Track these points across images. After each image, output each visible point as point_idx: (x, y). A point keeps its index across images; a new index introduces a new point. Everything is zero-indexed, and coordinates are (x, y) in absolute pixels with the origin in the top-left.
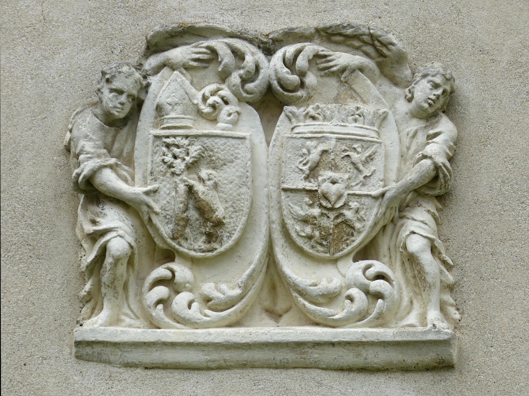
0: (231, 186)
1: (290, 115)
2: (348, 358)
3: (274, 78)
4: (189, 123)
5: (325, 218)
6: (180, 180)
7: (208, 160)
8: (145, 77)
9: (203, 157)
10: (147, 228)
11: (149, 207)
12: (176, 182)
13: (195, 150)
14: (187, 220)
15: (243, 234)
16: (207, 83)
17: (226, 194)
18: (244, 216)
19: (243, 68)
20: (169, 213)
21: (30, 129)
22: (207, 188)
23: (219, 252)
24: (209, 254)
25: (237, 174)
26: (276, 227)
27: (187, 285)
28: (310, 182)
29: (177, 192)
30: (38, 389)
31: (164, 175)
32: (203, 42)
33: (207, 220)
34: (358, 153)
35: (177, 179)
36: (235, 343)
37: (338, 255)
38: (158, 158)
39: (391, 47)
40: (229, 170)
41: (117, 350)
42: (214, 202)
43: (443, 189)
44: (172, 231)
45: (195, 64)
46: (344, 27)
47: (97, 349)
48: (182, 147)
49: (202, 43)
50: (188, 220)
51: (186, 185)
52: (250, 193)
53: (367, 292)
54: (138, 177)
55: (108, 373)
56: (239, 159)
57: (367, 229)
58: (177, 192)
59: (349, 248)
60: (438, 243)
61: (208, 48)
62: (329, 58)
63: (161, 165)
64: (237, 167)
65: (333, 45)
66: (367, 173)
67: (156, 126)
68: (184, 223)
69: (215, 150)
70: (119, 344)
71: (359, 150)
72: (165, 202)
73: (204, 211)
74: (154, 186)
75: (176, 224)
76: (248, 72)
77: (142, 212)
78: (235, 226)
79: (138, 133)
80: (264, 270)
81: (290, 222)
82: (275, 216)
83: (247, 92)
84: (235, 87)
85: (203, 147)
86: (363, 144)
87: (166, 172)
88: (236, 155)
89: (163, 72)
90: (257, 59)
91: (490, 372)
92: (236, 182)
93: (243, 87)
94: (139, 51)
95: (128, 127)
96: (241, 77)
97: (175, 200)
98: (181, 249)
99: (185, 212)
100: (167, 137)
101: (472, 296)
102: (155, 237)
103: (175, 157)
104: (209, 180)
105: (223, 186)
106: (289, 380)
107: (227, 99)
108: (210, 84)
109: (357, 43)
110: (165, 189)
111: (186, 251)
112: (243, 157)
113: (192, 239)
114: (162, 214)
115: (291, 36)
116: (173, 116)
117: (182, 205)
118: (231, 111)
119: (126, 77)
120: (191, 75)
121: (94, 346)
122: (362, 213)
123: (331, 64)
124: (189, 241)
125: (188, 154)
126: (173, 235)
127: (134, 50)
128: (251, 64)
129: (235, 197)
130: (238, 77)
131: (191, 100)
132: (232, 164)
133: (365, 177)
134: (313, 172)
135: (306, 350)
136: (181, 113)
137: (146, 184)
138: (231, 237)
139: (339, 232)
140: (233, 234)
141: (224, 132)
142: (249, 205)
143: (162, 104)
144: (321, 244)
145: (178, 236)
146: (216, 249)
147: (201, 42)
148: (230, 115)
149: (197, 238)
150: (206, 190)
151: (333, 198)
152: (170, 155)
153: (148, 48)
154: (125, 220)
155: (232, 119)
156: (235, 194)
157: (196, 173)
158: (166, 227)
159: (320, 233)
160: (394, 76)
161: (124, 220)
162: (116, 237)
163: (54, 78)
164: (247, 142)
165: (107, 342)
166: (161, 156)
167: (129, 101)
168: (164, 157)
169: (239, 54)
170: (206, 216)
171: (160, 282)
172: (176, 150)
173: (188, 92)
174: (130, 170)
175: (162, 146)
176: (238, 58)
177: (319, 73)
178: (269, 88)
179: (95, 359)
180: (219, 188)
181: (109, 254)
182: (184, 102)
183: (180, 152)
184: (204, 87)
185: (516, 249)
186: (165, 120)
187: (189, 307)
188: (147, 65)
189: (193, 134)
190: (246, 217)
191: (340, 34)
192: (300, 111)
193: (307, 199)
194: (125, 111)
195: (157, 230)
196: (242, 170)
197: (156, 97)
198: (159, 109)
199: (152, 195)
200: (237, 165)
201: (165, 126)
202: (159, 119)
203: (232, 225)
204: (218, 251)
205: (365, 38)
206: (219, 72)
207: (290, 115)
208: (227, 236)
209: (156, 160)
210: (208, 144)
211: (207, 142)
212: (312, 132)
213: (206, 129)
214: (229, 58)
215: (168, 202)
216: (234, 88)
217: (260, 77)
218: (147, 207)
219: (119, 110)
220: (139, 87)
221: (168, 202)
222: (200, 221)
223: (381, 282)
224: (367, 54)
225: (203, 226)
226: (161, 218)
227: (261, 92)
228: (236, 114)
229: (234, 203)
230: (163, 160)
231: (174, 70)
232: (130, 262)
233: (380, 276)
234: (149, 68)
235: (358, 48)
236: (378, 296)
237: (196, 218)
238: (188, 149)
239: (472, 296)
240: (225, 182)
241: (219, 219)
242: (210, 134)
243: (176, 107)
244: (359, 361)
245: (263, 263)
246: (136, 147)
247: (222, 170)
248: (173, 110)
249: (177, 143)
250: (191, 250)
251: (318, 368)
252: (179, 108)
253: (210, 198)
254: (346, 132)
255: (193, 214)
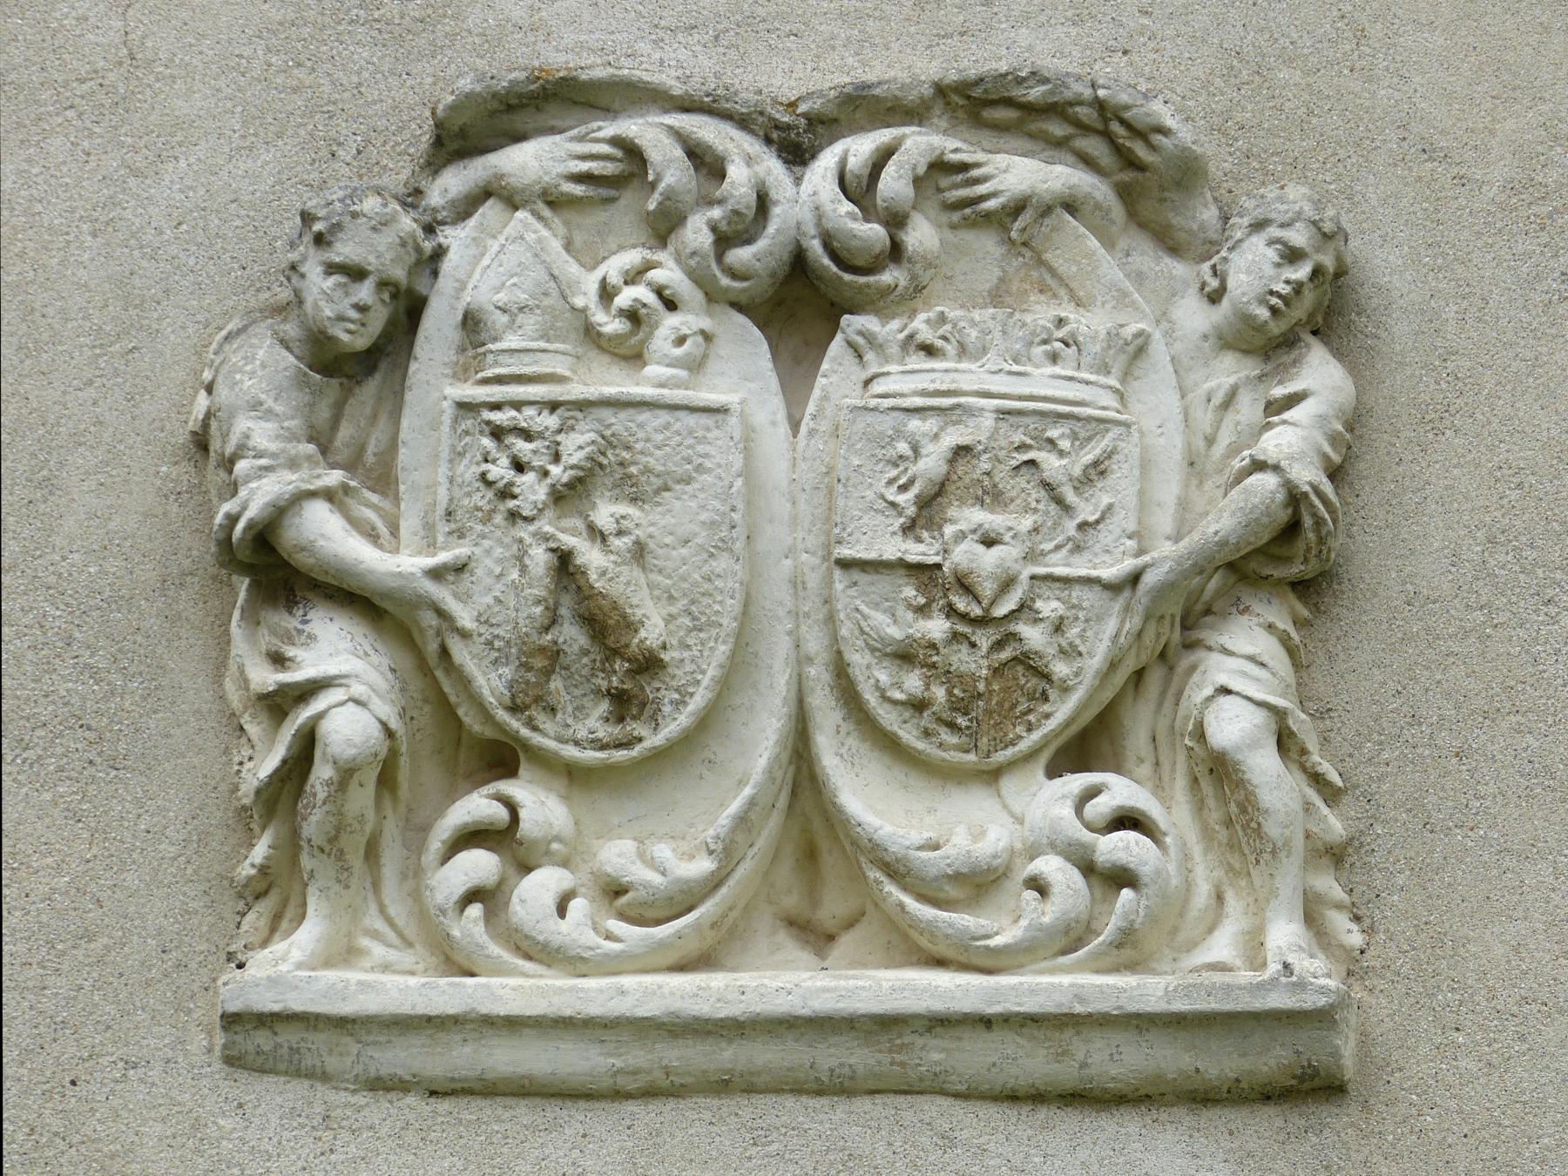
0: (684, 551)
1: (860, 340)
2: (1032, 1062)
3: (813, 232)
4: (560, 367)
5: (964, 648)
6: (534, 535)
7: (618, 476)
8: (429, 229)
9: (601, 466)
10: (435, 679)
11: (441, 613)
12: (521, 541)
13: (577, 445)
14: (554, 655)
15: (719, 695)
16: (614, 247)
17: (669, 577)
18: (724, 642)
19: (720, 202)
20: (502, 633)
21: (90, 383)
22: (612, 558)
23: (650, 750)
24: (621, 755)
25: (704, 517)
26: (819, 674)
27: (555, 846)
28: (919, 540)
29: (524, 570)
30: (113, 1156)
31: (487, 519)
32: (601, 123)
33: (614, 653)
34: (1062, 454)
35: (524, 532)
36: (696, 1019)
37: (1001, 756)
38: (468, 471)
39: (1158, 139)
40: (678, 504)
41: (348, 1039)
42: (635, 601)
43: (1313, 561)
44: (511, 685)
45: (578, 190)
46: (1020, 81)
47: (289, 1036)
48: (541, 435)
49: (600, 129)
50: (558, 652)
51: (553, 550)
52: (740, 574)
53: (1088, 868)
54: (409, 525)
55: (319, 1109)
56: (709, 471)
57: (1088, 679)
58: (524, 570)
59: (1036, 736)
60: (1300, 722)
61: (616, 141)
62: (975, 173)
63: (478, 490)
64: (702, 496)
65: (987, 133)
66: (1087, 513)
67: (462, 373)
68: (546, 663)
69: (639, 446)
70: (354, 1021)
71: (1065, 444)
72: (489, 600)
73: (604, 625)
74: (457, 551)
75: (522, 665)
76: (736, 212)
77: (421, 631)
78: (696, 671)
79: (408, 396)
80: (783, 802)
81: (858, 660)
82: (815, 643)
83: (733, 274)
84: (697, 259)
85: (603, 437)
86: (1077, 426)
87: (493, 511)
88: (700, 460)
89: (483, 215)
90: (762, 175)
91: (1453, 1104)
92: (699, 540)
93: (719, 257)
94: (412, 150)
95: (378, 376)
96: (714, 229)
97: (517, 595)
98: (537, 739)
99: (547, 629)
100: (496, 406)
101: (1400, 880)
102: (458, 705)
103: (519, 467)
104: (620, 533)
105: (660, 551)
106: (855, 1129)
107: (673, 295)
108: (621, 248)
109: (1058, 129)
110: (489, 562)
111: (551, 744)
112: (719, 465)
113: (570, 709)
114: (480, 635)
115: (862, 107)
116: (514, 345)
117: (538, 610)
118: (685, 331)
119: (374, 229)
120: (567, 224)
121: (278, 1028)
122: (1073, 632)
123: (981, 189)
124: (559, 715)
125: (556, 458)
126: (513, 697)
127: (398, 149)
128: (743, 190)
129: (696, 584)
130: (706, 230)
131: (565, 298)
132: (688, 488)
133: (1083, 526)
134: (928, 511)
135: (907, 1040)
136: (536, 335)
137: (432, 546)
138: (684, 703)
139: (1005, 690)
140: (692, 695)
141: (665, 392)
142: (738, 609)
143: (480, 310)
144: (952, 726)
145: (528, 700)
146: (640, 740)
147: (595, 125)
148: (681, 341)
149: (583, 707)
150: (612, 566)
151: (987, 589)
152: (504, 461)
153: (438, 142)
154: (371, 652)
155: (688, 354)
156: (696, 576)
157: (580, 513)
158: (493, 675)
159: (950, 693)
160: (1169, 226)
161: (366, 654)
162: (342, 704)
163: (159, 231)
164: (733, 420)
165: (318, 1016)
166: (478, 464)
167: (383, 301)
168: (485, 467)
169: (708, 159)
170: (610, 642)
171: (473, 837)
172: (522, 447)
173: (556, 273)
174: (386, 504)
175: (481, 432)
176: (704, 171)
177: (945, 218)
178: (799, 261)
179: (282, 1067)
180: (648, 558)
181: (324, 754)
182: (546, 302)
183: (535, 452)
184: (604, 258)
185: (1530, 739)
186: (490, 357)
187: (562, 911)
188: (436, 193)
189: (573, 398)
190: (730, 646)
191: (1009, 102)
192: (889, 330)
193: (909, 592)
194: (370, 329)
195: (465, 682)
196: (716, 504)
197: (462, 287)
198: (471, 323)
199: (451, 578)
200: (702, 490)
201: (489, 373)
202: (470, 353)
203: (689, 667)
204: (647, 744)
205: (1083, 112)
206: (648, 213)
207: (860, 340)
208: (671, 702)
209: (462, 475)
210: (618, 428)
211: (613, 420)
212: (924, 393)
213: (611, 382)
214: (678, 173)
215: (498, 601)
216: (692, 263)
217: (771, 229)
218: (435, 616)
219: (352, 327)
220: (411, 258)
221: (498, 601)
222: (592, 656)
223: (1129, 836)
224: (1087, 162)
225: (603, 671)
226: (478, 646)
227: (773, 275)
228: (700, 339)
229: (693, 602)
230: (483, 475)
231: (516, 208)
232: (387, 779)
233: (1127, 820)
234: (442, 202)
235: (1060, 144)
236: (1121, 878)
237: (581, 648)
238: (558, 444)
239: (1400, 880)
240: (667, 540)
241: (651, 651)
242: (624, 398)
243: (520, 318)
244: (1065, 1073)
245: (778, 781)
246: (402, 436)
247: (659, 504)
248: (512, 326)
249: (524, 424)
250: (567, 742)
251: (943, 1093)
252: (532, 321)
253: (622, 587)
254: (1026, 391)
255: (572, 635)
